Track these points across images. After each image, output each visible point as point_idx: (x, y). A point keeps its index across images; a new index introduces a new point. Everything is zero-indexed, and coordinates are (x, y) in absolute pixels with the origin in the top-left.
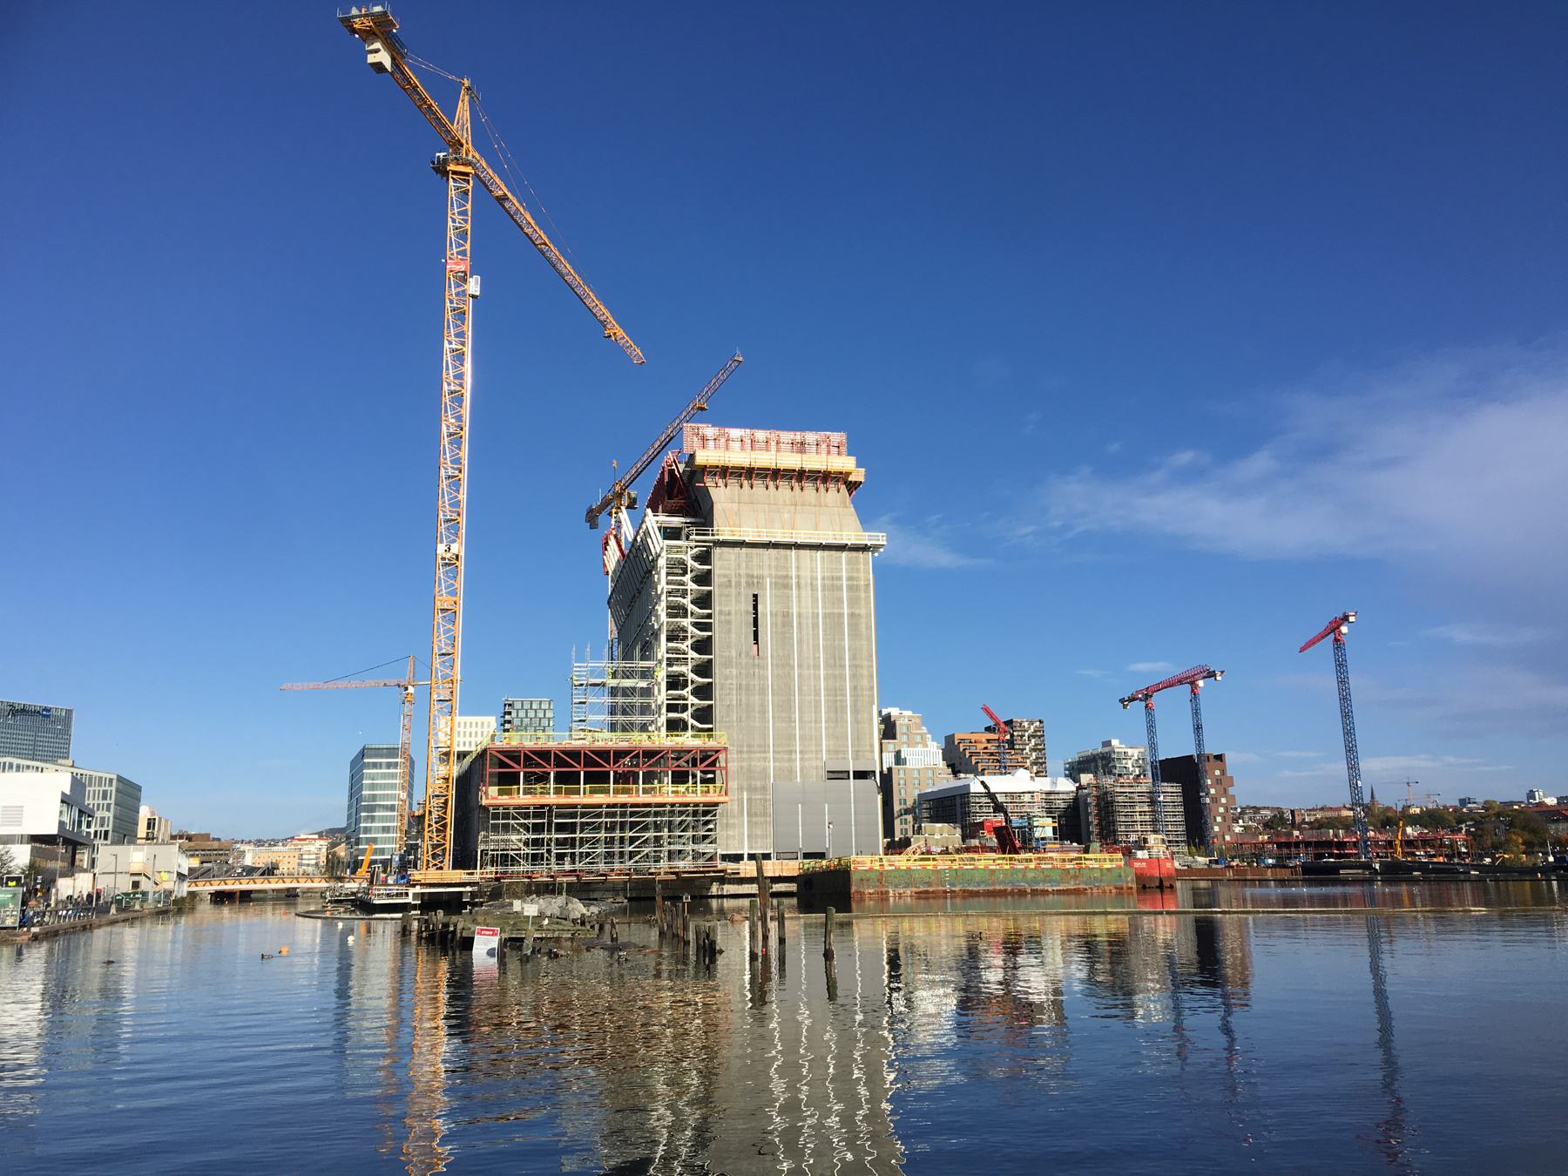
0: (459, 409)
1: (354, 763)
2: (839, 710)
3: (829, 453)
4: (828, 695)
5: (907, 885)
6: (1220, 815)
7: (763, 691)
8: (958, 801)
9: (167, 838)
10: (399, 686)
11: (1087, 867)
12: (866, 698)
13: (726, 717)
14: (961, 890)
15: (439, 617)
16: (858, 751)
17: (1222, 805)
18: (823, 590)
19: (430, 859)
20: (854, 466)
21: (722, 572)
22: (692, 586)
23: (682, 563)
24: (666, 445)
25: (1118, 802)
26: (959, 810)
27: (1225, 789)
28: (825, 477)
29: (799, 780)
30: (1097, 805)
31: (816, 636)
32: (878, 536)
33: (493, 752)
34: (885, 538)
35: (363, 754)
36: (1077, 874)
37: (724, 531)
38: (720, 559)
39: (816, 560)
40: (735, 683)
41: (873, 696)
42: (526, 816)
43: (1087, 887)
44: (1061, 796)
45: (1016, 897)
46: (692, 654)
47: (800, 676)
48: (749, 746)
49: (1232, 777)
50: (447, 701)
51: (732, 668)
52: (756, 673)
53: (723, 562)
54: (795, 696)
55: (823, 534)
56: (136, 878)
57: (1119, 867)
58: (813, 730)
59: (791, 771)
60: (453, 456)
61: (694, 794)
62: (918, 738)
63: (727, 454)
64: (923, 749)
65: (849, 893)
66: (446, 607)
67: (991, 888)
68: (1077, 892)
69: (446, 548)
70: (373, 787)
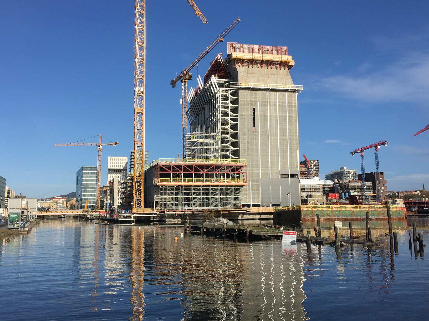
1: (78, 173)
2: (285, 152)
7: (257, 145)
9: (14, 197)
10: (96, 145)
14: (341, 218)
18: (279, 107)
22: (230, 105)
24: (205, 55)
25: (350, 188)
28: (280, 64)
31: (276, 124)
32: (300, 86)
35: (82, 169)
36: (384, 213)
37: (243, 84)
38: (241, 95)
39: (276, 95)
40: (246, 141)
44: (328, 186)
45: (362, 221)
46: (231, 130)
48: (252, 165)
50: (140, 147)
53: (242, 96)
56: (23, 210)
57: (399, 210)
59: (268, 174)
63: (244, 54)
67: (352, 218)
69: (139, 89)
70: (86, 181)
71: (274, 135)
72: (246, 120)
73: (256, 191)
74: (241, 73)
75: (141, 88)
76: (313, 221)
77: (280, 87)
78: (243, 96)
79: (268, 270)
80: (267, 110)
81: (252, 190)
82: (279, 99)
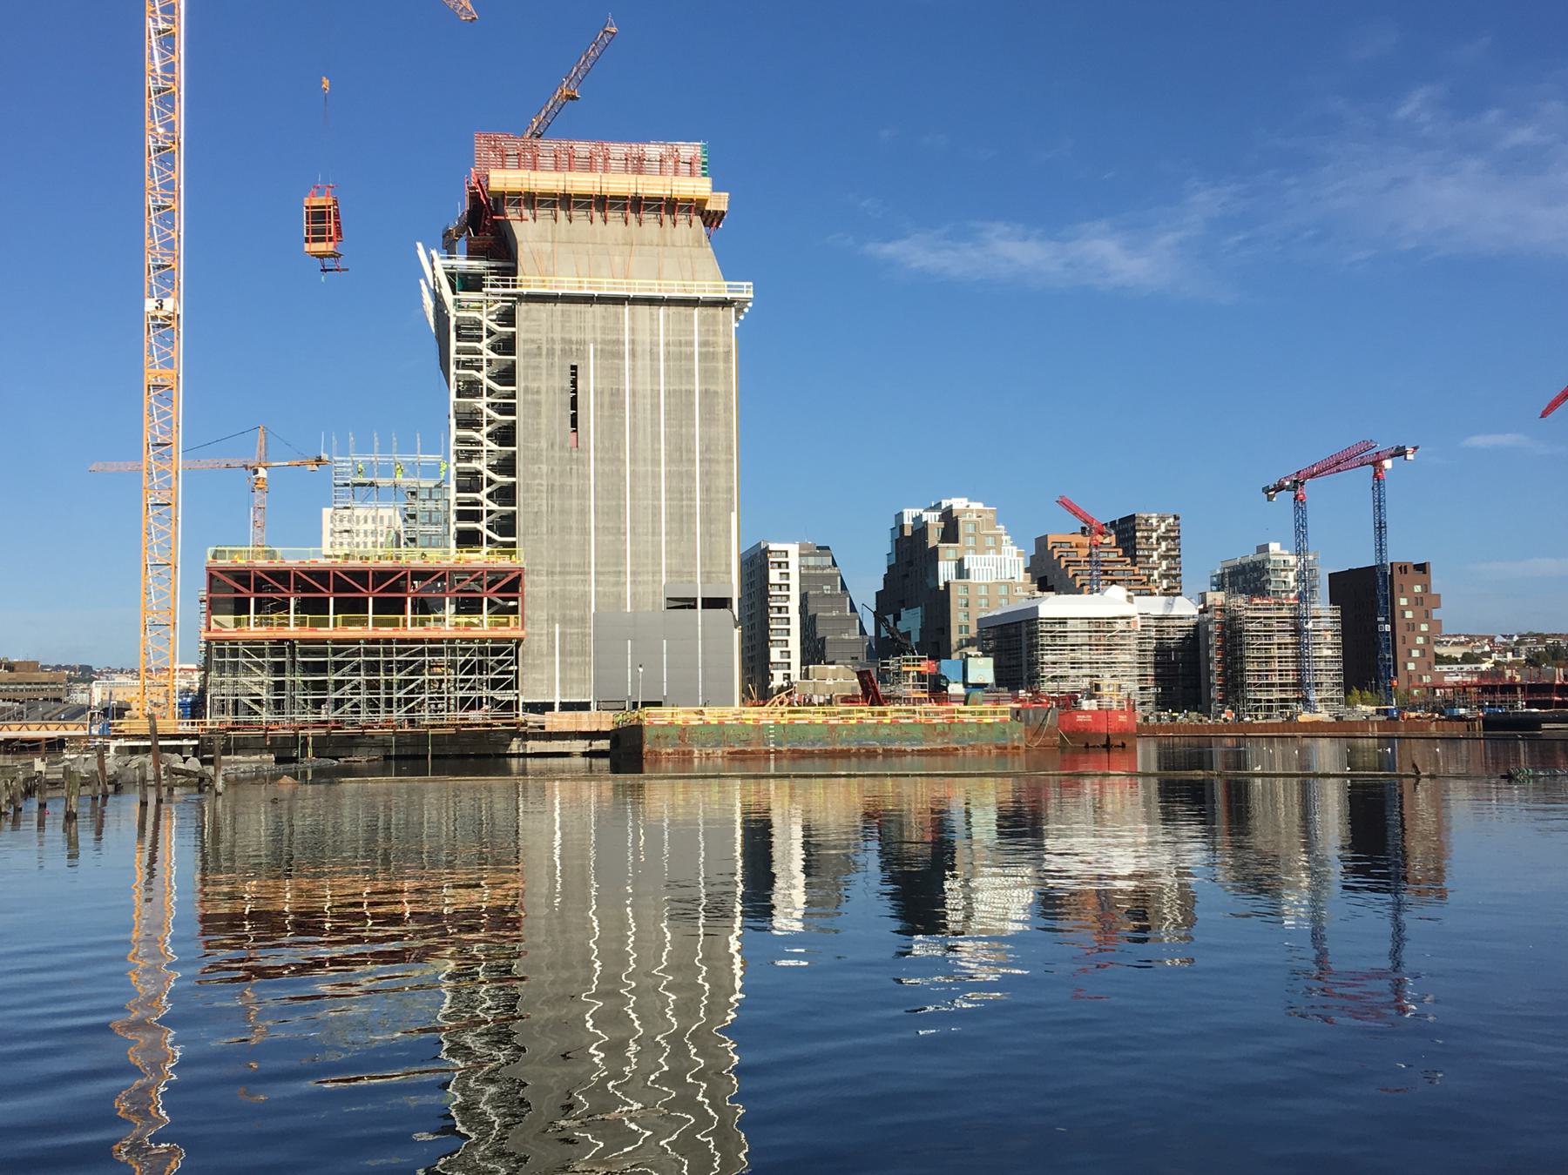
0: (170, 114)
2: (685, 518)
3: (676, 173)
4: (671, 499)
6: (1417, 647)
7: (583, 494)
8: (1024, 630)
11: (961, 722)
12: (722, 503)
13: (533, 528)
14: (789, 750)
15: (150, 399)
16: (709, 572)
17: (1422, 634)
18: (667, 360)
20: (709, 190)
22: (489, 354)
23: (478, 325)
26: (1025, 643)
27: (1427, 611)
28: (669, 206)
29: (629, 610)
30: (1222, 635)
32: (742, 286)
33: (258, 573)
34: (751, 289)
36: (947, 728)
37: (529, 281)
38: (526, 319)
40: (544, 483)
41: (731, 500)
42: (260, 654)
43: (958, 746)
44: (1177, 623)
45: (863, 758)
47: (633, 474)
48: (563, 565)
49: (1438, 596)
51: (542, 463)
52: (574, 471)
53: (532, 324)
55: (666, 285)
57: (1004, 722)
58: (650, 544)
59: (620, 598)
60: (164, 178)
61: (484, 626)
62: (990, 542)
64: (995, 556)
65: (641, 753)
66: (159, 383)
68: (944, 752)
69: (157, 304)
71: (645, 460)
72: (543, 410)
73: (577, 655)
74: (527, 241)
75: (164, 300)
77: (666, 291)
78: (533, 323)
80: (622, 371)
82: (667, 330)
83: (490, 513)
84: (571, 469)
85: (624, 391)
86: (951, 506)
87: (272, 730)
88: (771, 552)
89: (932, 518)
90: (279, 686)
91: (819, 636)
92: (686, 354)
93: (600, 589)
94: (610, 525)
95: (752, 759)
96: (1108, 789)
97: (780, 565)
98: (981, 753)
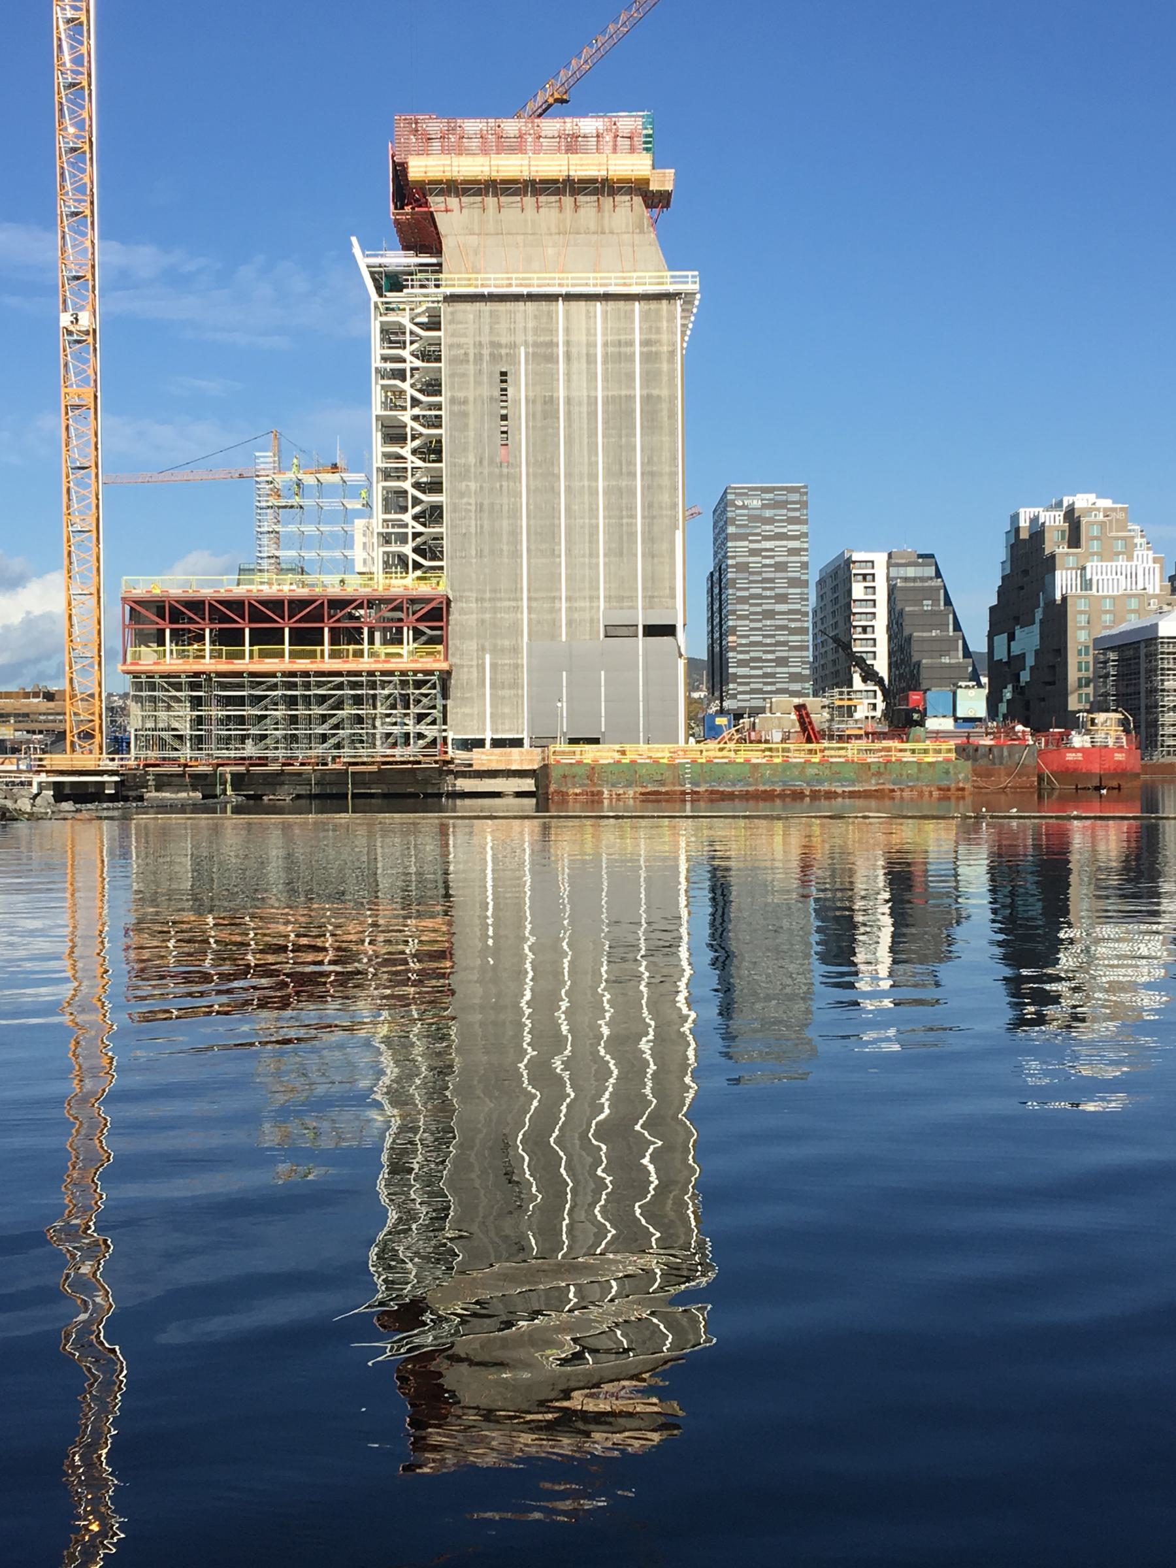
2: (625, 537)
4: (610, 517)
5: (629, 784)
7: (515, 513)
8: (1143, 651)
11: (899, 761)
12: (666, 521)
14: (707, 791)
16: (653, 597)
18: (605, 362)
19: (76, 739)
21: (455, 340)
29: (564, 639)
31: (593, 433)
32: (687, 277)
38: (452, 322)
39: (595, 317)
40: (473, 501)
42: (178, 687)
43: (895, 787)
47: (568, 489)
48: (494, 591)
52: (505, 488)
54: (559, 519)
57: (948, 760)
60: (76, 182)
64: (1125, 563)
69: (72, 319)
73: (510, 688)
75: (80, 314)
76: (593, 802)
78: (460, 326)
79: (548, 972)
80: (556, 376)
81: (493, 686)
82: (605, 329)
83: (416, 535)
84: (501, 486)
85: (558, 399)
86: (1073, 503)
87: (191, 766)
88: (854, 562)
89: (1053, 520)
90: (199, 721)
91: (914, 660)
92: (626, 354)
93: (533, 616)
94: (544, 546)
95: (667, 801)
96: (1100, 833)
97: (865, 576)
98: (921, 794)
